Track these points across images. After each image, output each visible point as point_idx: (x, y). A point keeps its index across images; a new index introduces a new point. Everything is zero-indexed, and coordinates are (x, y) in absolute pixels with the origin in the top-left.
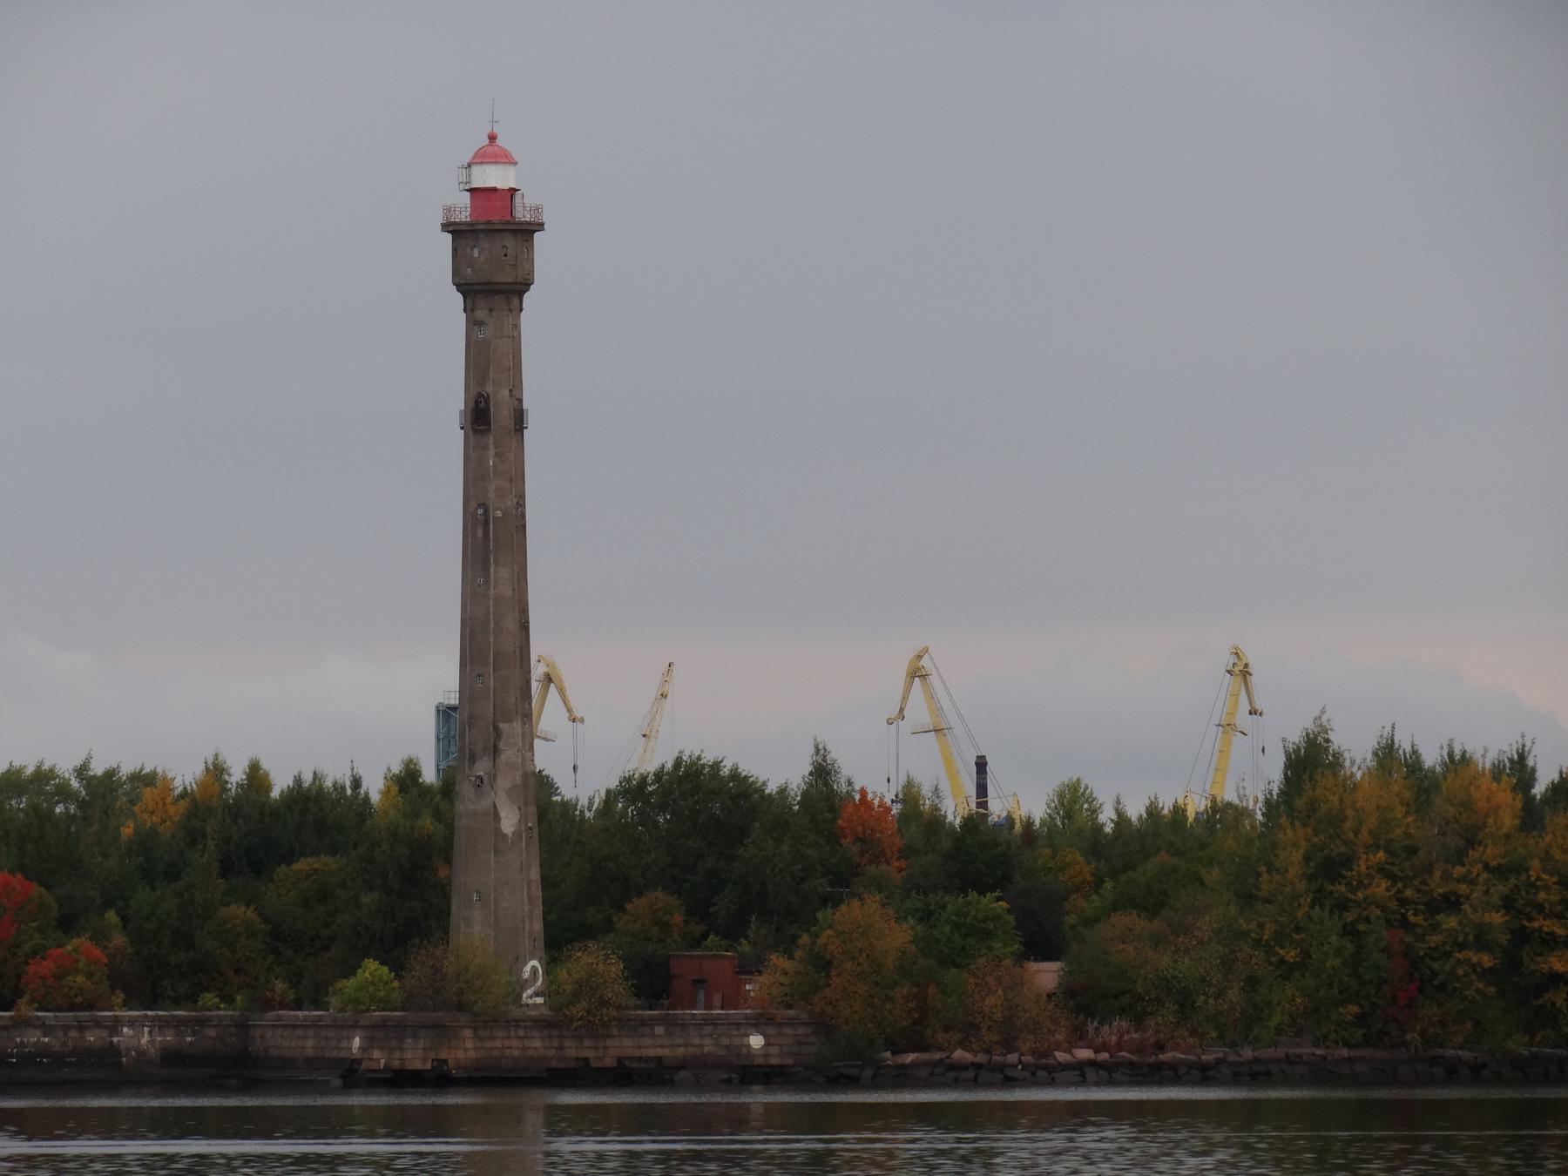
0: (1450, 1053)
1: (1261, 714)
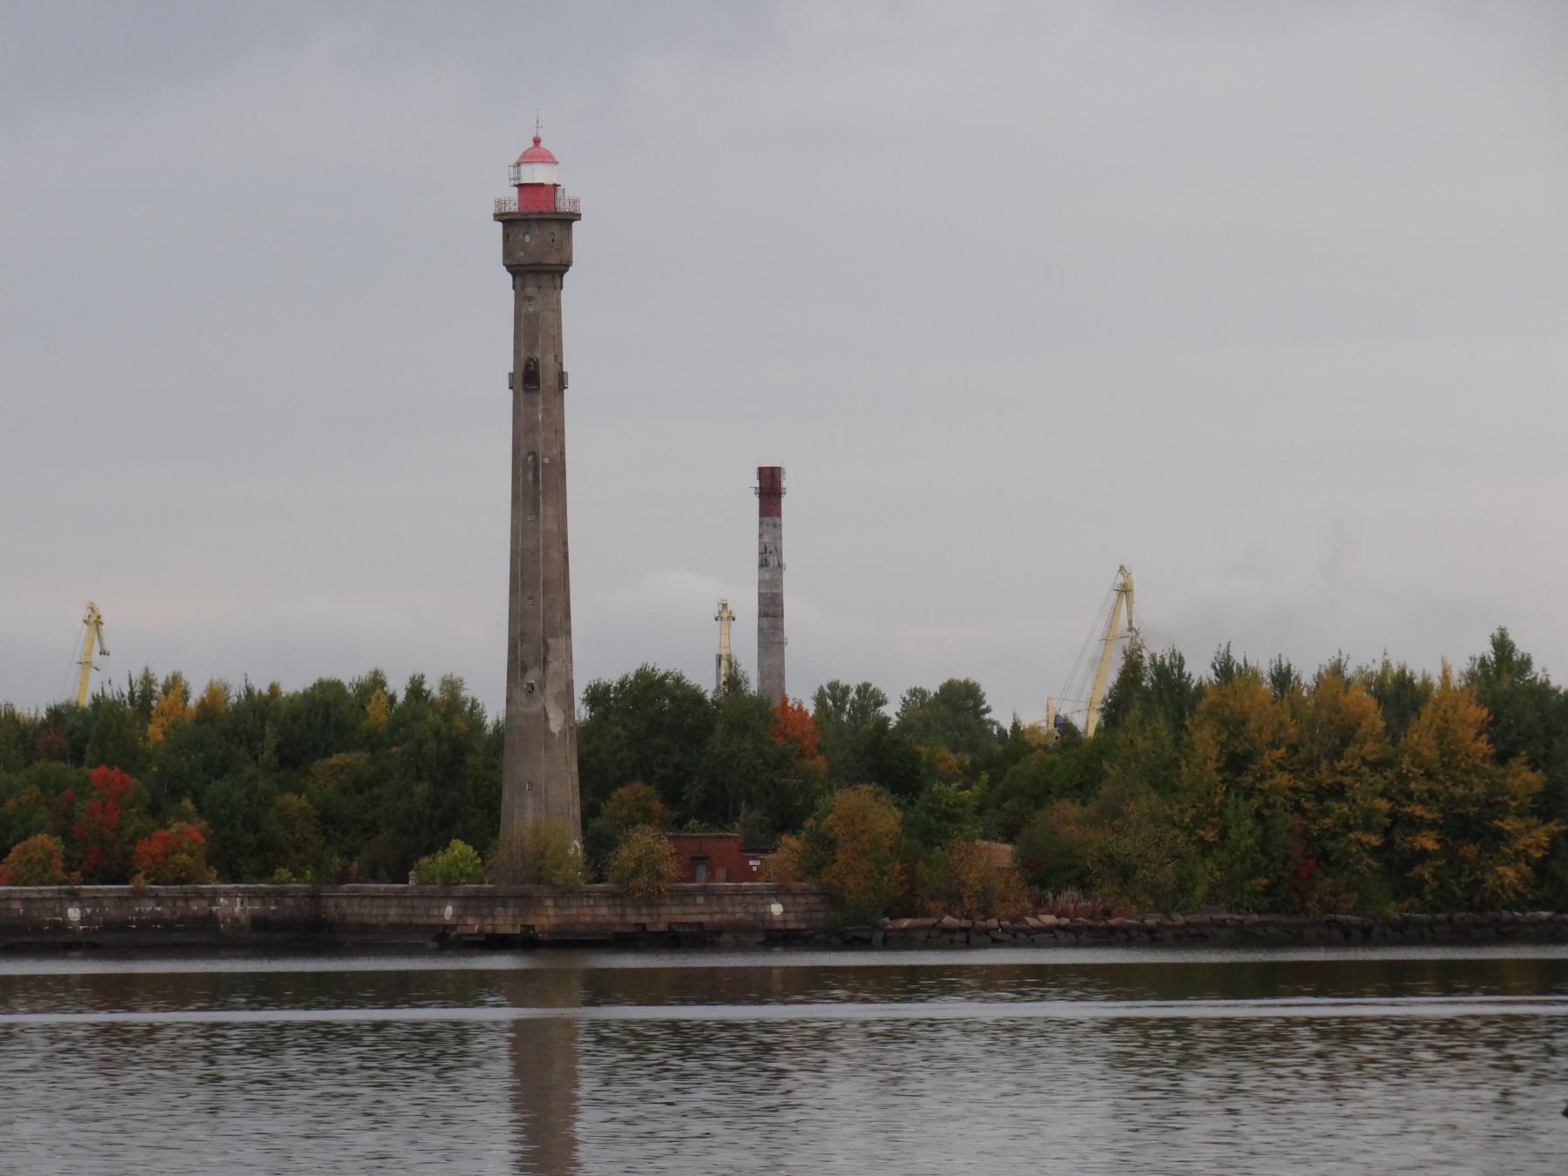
0: (1340, 917)
1: (108, 655)
